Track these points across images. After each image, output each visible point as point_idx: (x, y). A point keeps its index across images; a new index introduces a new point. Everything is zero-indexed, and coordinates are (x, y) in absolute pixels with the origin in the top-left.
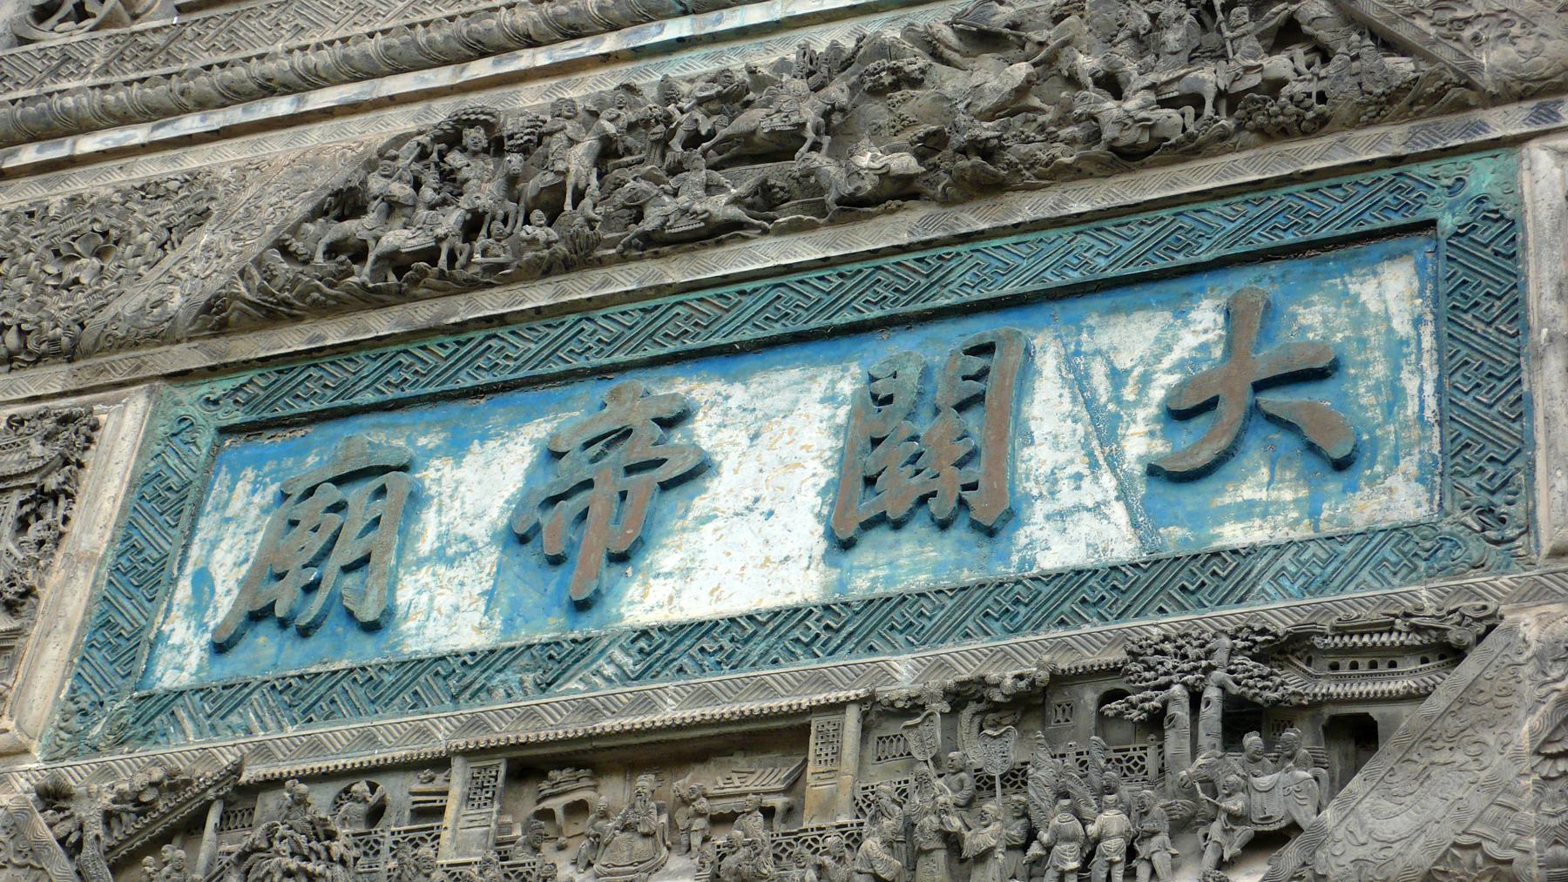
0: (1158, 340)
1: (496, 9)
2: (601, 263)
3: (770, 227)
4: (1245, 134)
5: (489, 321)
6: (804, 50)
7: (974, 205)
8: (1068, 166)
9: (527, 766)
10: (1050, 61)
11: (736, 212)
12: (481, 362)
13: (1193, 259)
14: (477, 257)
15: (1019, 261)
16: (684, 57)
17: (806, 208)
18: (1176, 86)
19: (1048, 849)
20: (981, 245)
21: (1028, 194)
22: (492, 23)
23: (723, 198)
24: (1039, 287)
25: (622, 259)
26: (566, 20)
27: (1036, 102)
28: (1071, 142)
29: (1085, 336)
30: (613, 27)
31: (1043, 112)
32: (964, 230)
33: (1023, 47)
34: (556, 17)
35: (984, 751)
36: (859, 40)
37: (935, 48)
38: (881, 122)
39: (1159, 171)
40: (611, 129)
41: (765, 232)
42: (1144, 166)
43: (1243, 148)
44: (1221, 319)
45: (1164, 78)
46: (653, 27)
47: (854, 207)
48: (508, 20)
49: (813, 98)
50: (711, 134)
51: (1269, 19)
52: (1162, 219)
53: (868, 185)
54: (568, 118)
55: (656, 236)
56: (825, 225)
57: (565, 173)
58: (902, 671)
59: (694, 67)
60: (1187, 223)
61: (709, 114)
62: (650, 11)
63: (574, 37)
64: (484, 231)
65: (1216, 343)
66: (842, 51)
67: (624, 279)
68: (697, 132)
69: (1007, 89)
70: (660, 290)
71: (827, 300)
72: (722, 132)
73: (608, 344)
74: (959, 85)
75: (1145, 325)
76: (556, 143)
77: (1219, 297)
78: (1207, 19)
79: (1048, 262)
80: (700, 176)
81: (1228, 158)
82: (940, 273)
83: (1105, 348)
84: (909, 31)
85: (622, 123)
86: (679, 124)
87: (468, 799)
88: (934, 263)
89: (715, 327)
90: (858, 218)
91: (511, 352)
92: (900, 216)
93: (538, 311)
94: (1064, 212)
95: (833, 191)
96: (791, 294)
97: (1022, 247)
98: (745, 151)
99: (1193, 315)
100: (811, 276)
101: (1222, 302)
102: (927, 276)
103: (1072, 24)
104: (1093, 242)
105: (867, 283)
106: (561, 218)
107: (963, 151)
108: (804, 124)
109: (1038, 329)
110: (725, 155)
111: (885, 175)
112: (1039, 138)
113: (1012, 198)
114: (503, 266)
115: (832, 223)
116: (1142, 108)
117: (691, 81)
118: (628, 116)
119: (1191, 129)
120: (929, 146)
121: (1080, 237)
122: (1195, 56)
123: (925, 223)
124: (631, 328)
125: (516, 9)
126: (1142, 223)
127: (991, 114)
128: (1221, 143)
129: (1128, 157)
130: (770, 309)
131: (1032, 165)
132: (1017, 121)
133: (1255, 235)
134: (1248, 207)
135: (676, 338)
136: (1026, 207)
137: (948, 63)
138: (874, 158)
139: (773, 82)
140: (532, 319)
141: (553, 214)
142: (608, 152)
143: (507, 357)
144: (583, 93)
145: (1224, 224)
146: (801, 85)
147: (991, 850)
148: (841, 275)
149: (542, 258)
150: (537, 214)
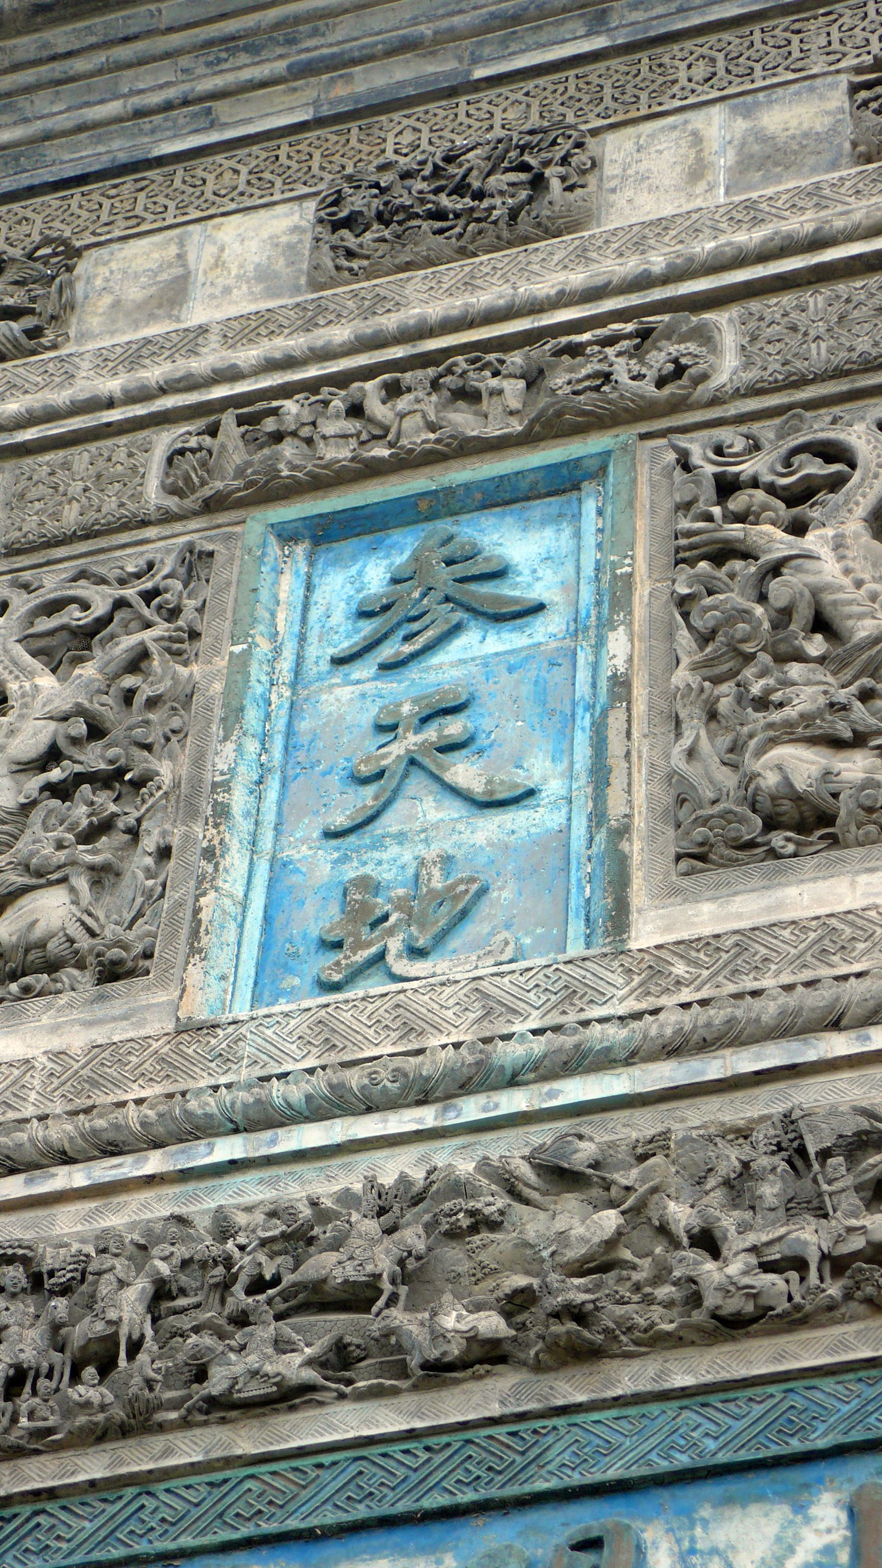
0: (779, 1539)
1: (27, 1121)
2: (161, 1428)
3: (348, 1390)
4: (853, 1305)
5: (37, 1494)
6: (371, 1182)
7: (570, 1371)
8: (669, 1334)
10: (638, 1210)
11: (310, 1375)
12: (29, 1543)
13: (808, 1446)
14: (24, 1422)
15: (621, 1439)
16: (236, 1180)
17: (384, 1370)
18: (777, 1247)
20: (579, 1419)
21: (627, 1362)
22: (22, 1137)
23: (297, 1359)
24: (645, 1471)
25: (185, 1423)
26: (105, 1136)
27: (627, 1254)
28: (669, 1304)
29: (698, 1531)
30: (157, 1145)
31: (634, 1267)
32: (560, 1402)
33: (608, 1189)
34: (94, 1132)
36: (429, 1173)
37: (513, 1185)
38: (460, 1269)
39: (766, 1342)
40: (164, 1269)
41: (342, 1396)
42: (748, 1335)
43: (853, 1319)
44: (844, 1517)
45: (765, 1238)
46: (201, 1146)
47: (439, 1372)
48: (40, 1134)
49: (387, 1240)
50: (276, 1280)
51: (866, 1171)
52: (772, 1396)
53: (455, 1350)
54: (116, 1255)
55: (223, 1399)
56: (408, 1390)
57: (117, 1323)
59: (250, 1192)
60: (798, 1402)
61: (272, 1256)
62: (197, 1128)
63: (113, 1154)
64: (28, 1388)
65: (841, 1546)
66: (411, 1184)
67: (189, 1449)
68: (261, 1276)
69: (596, 1240)
70: (229, 1462)
71: (415, 1478)
72: (288, 1279)
73: (173, 1524)
74: (542, 1228)
75: (763, 1521)
76: (105, 1287)
77: (840, 1490)
78: (799, 1163)
79: (653, 1441)
80: (265, 1331)
81: (837, 1331)
82: (536, 1451)
83: (721, 1546)
84: (484, 1165)
85: (176, 1261)
86: (241, 1268)
88: (530, 1439)
89: (291, 1507)
90: (444, 1384)
91: (62, 1531)
92: (489, 1382)
93: (92, 1484)
94: (667, 1386)
95: (417, 1354)
96: (374, 1469)
97: (623, 1423)
98: (315, 1298)
99: (814, 1511)
100: (394, 1449)
101: (845, 1496)
102: (523, 1453)
103: (657, 1165)
104: (700, 1420)
105: (457, 1459)
106: (114, 1375)
107: (556, 1315)
108: (380, 1275)
109: (648, 1520)
110: (292, 1303)
111: (472, 1338)
112: (636, 1298)
113: (610, 1366)
114: (50, 1431)
115: (415, 1388)
116: (745, 1273)
117: (248, 1209)
118: (181, 1252)
119: (797, 1299)
120: (516, 1304)
121: (686, 1414)
122: (792, 1207)
123: (516, 1392)
124: (197, 1505)
125: (49, 1122)
126: (751, 1399)
127: (580, 1268)
128: (830, 1313)
129: (732, 1326)
130: (352, 1486)
131: (629, 1329)
132: (610, 1278)
133: (872, 1420)
134: (861, 1386)
135: (249, 1519)
136: (629, 1377)
137: (527, 1202)
138: (459, 1318)
139: (337, 1215)
140: (86, 1492)
141: (107, 1366)
142: (161, 1293)
143: (58, 1538)
144: (126, 1219)
145: (838, 1405)
146: (372, 1226)
148: (428, 1449)
149: (96, 1424)
150: (90, 1372)
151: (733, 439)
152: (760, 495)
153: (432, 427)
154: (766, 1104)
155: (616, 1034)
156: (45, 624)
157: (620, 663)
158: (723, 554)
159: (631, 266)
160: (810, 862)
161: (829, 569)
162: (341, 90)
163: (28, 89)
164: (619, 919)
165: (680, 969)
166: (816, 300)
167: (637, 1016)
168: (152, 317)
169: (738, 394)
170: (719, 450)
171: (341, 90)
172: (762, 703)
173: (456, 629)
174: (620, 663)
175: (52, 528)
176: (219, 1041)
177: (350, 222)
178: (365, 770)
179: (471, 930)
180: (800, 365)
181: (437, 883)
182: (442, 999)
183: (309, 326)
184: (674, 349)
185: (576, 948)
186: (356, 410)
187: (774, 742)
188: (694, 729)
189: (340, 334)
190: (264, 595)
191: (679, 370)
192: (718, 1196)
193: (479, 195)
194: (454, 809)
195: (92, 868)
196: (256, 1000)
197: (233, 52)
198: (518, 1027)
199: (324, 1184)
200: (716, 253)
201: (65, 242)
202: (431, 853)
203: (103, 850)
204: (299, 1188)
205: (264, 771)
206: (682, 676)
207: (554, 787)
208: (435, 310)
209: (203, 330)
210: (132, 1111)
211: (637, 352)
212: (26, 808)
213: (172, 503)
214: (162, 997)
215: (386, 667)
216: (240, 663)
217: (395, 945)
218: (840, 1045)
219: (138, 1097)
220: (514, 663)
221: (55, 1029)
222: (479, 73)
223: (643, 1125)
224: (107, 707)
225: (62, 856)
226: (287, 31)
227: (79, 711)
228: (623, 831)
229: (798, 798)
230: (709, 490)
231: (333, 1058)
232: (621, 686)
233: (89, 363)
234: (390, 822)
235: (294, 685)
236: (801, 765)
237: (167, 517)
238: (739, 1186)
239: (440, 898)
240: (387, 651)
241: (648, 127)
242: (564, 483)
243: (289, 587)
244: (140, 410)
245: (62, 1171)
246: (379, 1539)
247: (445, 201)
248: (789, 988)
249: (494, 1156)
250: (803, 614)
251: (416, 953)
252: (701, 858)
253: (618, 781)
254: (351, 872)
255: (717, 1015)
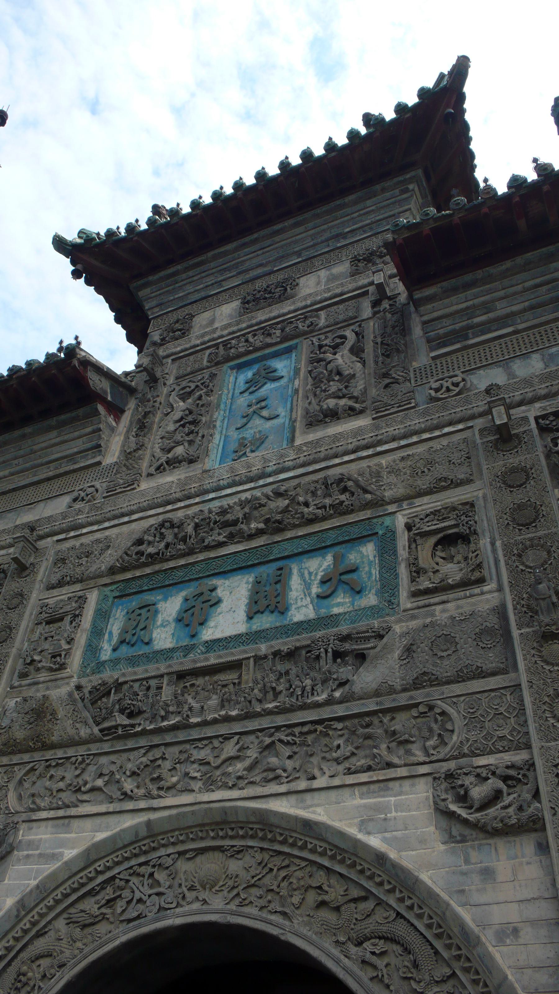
2: (196, 553)
6: (240, 500)
9: (181, 676)
11: (225, 539)
17: (240, 538)
19: (294, 690)
25: (200, 552)
27: (291, 509)
28: (298, 518)
30: (198, 496)
35: (281, 667)
39: (318, 524)
40: (197, 521)
43: (336, 517)
46: (207, 495)
47: (251, 537)
50: (219, 521)
57: (187, 532)
58: (263, 648)
59: (217, 503)
60: (324, 536)
67: (201, 557)
84: (262, 493)
87: (168, 685)
90: (252, 539)
107: (274, 522)
111: (257, 529)
118: (201, 517)
120: (267, 521)
128: (331, 517)
132: (286, 514)
136: (289, 534)
137: (271, 500)
142: (197, 526)
147: (282, 691)
151: (323, 337)
152: (327, 348)
153: (261, 342)
154: (321, 475)
155: (290, 463)
156: (182, 392)
157: (297, 386)
158: (319, 360)
159: (304, 303)
160: (333, 423)
161: (340, 361)
162: (247, 276)
163: (185, 285)
164: (292, 439)
165: (305, 448)
166: (341, 307)
167: (295, 459)
168: (208, 327)
169: (324, 328)
170: (319, 339)
171: (247, 276)
172: (325, 391)
173: (265, 383)
174: (297, 386)
175: (185, 372)
176: (211, 473)
177: (248, 302)
178: (245, 415)
179: (264, 446)
180: (337, 320)
181: (258, 437)
182: (255, 460)
183: (238, 324)
184: (311, 320)
185: (285, 446)
186: (247, 341)
187: (327, 399)
188: (311, 397)
189: (244, 325)
190: (226, 381)
191: (312, 323)
192: (310, 495)
193: (274, 293)
194: (262, 421)
195: (188, 441)
196: (220, 464)
197: (225, 271)
198: (271, 464)
199: (231, 501)
200: (320, 299)
201: (191, 314)
202: (256, 430)
203: (191, 437)
204: (225, 503)
205: (224, 417)
206: (309, 387)
207: (283, 414)
208: (263, 318)
209: (217, 328)
210: (193, 490)
211: (304, 322)
212: (176, 430)
213: (209, 364)
214: (200, 466)
215: (251, 393)
216: (220, 396)
217: (248, 450)
218: (337, 461)
219: (194, 486)
220: (276, 389)
221: (179, 475)
222: (275, 269)
223: (296, 481)
224: (193, 408)
225: (182, 439)
226: (236, 266)
227: (187, 409)
228: (295, 421)
229: (331, 410)
230: (317, 348)
231: (233, 474)
232: (297, 391)
233: (194, 338)
234: (249, 425)
235: (232, 399)
236: (331, 403)
237: (208, 367)
238: (314, 493)
239: (258, 439)
240: (251, 390)
241: (309, 276)
242: (288, 351)
243: (232, 379)
244: (204, 346)
245: (179, 503)
246: (239, 572)
247: (266, 295)
248: (327, 450)
249: (265, 492)
250: (334, 371)
251: (253, 451)
252: (311, 425)
253: (294, 411)
254: (241, 436)
255: (311, 457)
